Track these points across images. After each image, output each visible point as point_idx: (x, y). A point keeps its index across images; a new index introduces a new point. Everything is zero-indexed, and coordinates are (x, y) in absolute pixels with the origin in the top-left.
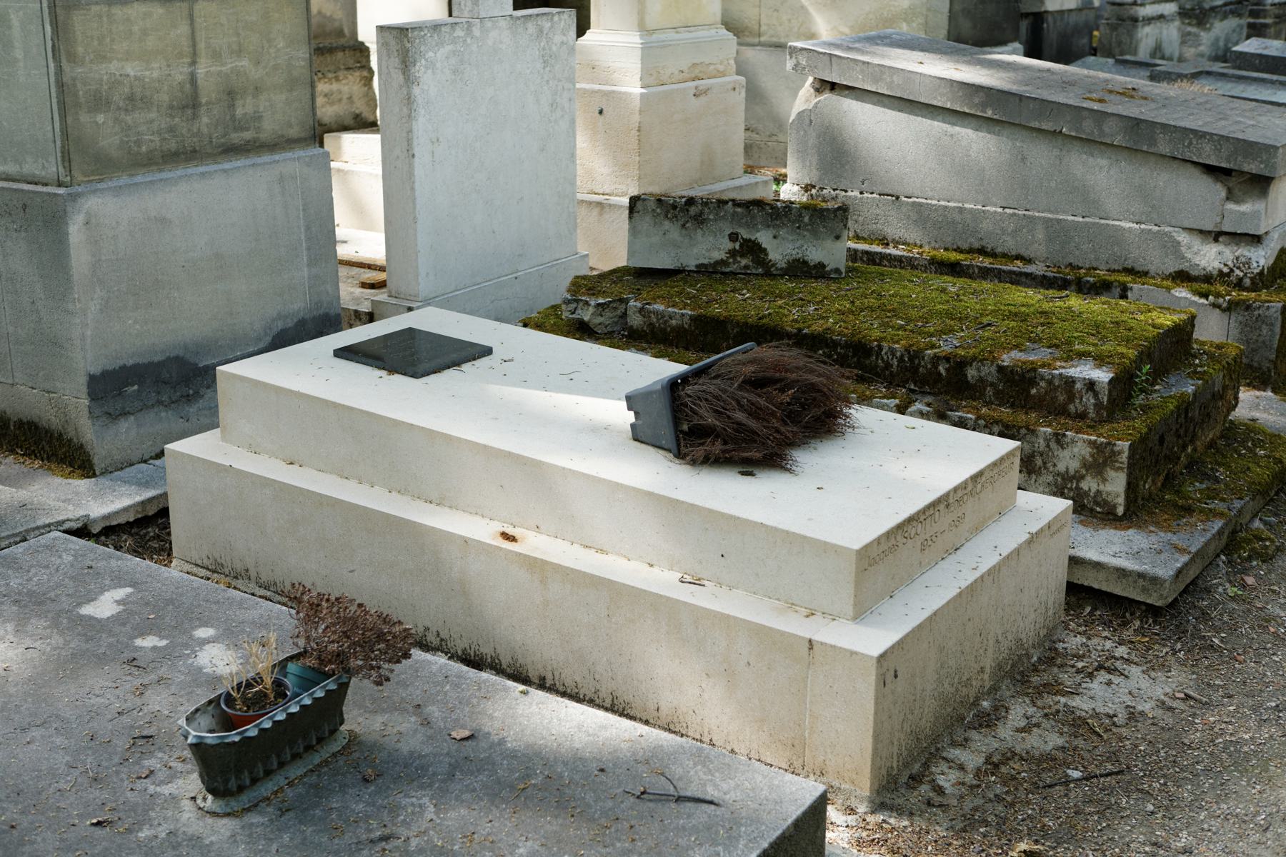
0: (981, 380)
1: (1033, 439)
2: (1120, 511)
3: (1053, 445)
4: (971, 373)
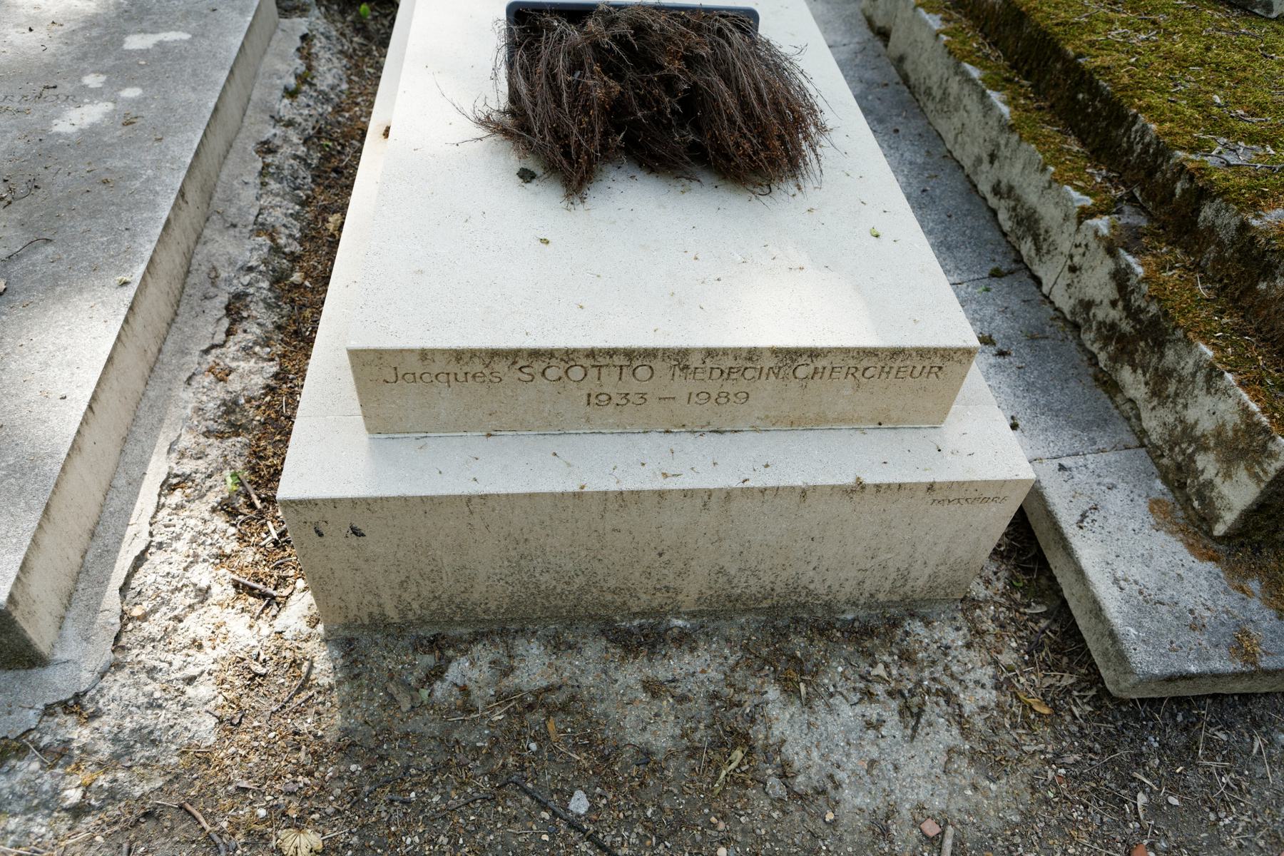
0: (1211, 229)
1: (1184, 353)
2: (1220, 529)
3: (1200, 378)
4: (1207, 212)
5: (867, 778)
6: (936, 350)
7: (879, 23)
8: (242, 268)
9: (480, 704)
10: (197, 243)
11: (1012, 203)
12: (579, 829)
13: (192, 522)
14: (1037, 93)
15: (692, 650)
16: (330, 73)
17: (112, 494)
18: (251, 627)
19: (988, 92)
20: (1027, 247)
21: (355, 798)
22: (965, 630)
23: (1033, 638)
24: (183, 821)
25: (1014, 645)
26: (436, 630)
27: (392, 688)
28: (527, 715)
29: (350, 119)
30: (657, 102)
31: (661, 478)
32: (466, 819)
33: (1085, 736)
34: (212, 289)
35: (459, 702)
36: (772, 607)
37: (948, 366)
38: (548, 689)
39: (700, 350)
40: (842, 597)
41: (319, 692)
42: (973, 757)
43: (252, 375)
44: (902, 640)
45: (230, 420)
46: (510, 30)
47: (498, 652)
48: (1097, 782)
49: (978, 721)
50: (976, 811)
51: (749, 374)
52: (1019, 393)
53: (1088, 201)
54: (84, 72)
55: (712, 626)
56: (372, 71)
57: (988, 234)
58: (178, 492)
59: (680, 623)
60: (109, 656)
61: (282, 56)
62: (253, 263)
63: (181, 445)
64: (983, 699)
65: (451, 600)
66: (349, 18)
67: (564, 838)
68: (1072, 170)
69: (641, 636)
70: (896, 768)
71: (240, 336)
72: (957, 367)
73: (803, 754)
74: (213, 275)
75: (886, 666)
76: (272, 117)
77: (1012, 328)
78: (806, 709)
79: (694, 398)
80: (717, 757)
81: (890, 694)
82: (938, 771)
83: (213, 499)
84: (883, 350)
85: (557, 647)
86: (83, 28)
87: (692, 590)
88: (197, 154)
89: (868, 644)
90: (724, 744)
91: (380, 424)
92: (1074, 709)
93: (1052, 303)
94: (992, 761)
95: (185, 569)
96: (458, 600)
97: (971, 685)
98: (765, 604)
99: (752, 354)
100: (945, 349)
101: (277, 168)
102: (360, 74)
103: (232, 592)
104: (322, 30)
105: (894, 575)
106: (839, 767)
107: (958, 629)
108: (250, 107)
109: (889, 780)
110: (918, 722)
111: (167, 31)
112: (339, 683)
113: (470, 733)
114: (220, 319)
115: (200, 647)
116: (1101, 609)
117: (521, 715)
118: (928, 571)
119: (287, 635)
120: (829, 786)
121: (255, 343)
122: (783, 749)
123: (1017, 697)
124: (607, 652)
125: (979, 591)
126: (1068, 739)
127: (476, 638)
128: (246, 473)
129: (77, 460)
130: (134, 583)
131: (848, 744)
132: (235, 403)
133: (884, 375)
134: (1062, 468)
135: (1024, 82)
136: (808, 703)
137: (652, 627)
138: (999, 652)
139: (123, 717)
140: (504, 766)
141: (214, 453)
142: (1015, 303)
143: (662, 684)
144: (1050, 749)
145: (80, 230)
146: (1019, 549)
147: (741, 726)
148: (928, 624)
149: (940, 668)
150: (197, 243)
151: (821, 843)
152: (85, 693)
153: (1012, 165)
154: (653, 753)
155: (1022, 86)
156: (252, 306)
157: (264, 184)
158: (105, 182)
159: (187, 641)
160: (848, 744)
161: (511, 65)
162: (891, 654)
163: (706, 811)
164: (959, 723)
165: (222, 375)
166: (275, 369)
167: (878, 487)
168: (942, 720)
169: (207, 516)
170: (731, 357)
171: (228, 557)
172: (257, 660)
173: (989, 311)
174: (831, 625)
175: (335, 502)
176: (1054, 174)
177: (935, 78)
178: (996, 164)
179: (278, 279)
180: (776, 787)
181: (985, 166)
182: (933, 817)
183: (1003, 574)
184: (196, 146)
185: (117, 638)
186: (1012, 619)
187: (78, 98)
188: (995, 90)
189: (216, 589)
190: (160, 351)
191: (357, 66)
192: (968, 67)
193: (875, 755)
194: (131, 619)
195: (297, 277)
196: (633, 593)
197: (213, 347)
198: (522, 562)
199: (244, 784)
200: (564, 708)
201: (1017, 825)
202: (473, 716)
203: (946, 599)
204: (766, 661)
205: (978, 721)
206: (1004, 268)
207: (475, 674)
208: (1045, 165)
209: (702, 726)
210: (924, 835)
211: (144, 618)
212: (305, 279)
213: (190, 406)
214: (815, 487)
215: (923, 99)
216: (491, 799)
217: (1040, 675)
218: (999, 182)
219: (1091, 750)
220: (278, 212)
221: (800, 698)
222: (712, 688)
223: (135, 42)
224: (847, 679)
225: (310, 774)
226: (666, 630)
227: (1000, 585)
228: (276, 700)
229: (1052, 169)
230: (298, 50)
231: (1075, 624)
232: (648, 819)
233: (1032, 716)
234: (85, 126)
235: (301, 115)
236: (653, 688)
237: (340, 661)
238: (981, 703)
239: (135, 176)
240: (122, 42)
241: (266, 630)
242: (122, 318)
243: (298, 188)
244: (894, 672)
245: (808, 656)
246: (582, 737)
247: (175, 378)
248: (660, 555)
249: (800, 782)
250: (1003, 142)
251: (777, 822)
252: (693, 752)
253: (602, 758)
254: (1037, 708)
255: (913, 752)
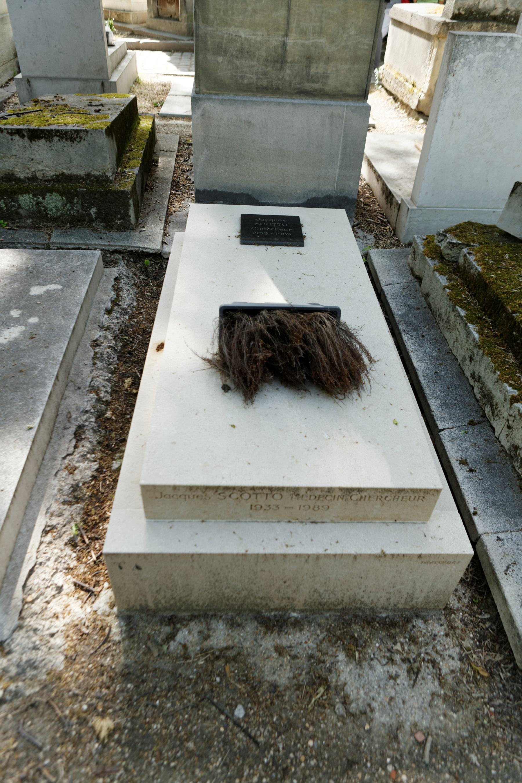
5: (388, 707)
6: (420, 490)
7: (417, 273)
8: (82, 411)
9: (192, 655)
10: (62, 399)
11: (481, 385)
12: (239, 726)
13: (56, 551)
14: (494, 326)
15: (301, 630)
16: (128, 298)
17: (20, 537)
18: (82, 607)
19: (469, 324)
20: (487, 410)
21: (129, 702)
22: (445, 626)
23: (482, 633)
24: (48, 709)
25: (471, 636)
26: (172, 613)
27: (149, 644)
28: (216, 662)
29: (137, 323)
30: (290, 358)
31: (285, 547)
32: (184, 717)
33: (506, 690)
34: (68, 424)
35: (182, 653)
36: (343, 609)
37: (427, 496)
38: (227, 648)
39: (305, 488)
40: (379, 605)
41: (114, 644)
42: (445, 699)
43: (86, 469)
44: (411, 630)
45: (74, 496)
46: (220, 322)
47: (202, 627)
48: (510, 717)
49: (449, 679)
50: (445, 729)
51: (328, 498)
52: (479, 494)
53: (516, 393)
54: (11, 309)
55: (312, 617)
56: (149, 294)
57: (468, 400)
58: (49, 535)
59: (295, 615)
60: (16, 622)
61: (105, 291)
62: (88, 409)
63: (51, 510)
64: (453, 666)
65: (180, 599)
66: (138, 265)
67: (231, 730)
68: (508, 374)
69: (275, 621)
70: (404, 702)
71: (81, 449)
72: (432, 497)
73: (355, 691)
74: (69, 416)
75: (402, 644)
76: (99, 326)
77: (478, 456)
78: (358, 667)
79: (302, 507)
80: (311, 690)
81: (403, 660)
82: (426, 705)
83: (66, 538)
84: (394, 489)
85: (232, 625)
86: (10, 283)
87: (301, 599)
88: (65, 355)
89: (393, 631)
90: (314, 683)
91: (152, 514)
92: (501, 674)
93: (500, 442)
94: (455, 701)
95: (52, 576)
96: (184, 600)
97: (447, 657)
98: (339, 607)
99: (330, 490)
100: (425, 489)
101: (101, 354)
102: (143, 296)
103: (73, 588)
104: (125, 273)
105: (405, 596)
106: (373, 699)
107: (442, 625)
108: (89, 321)
109: (400, 709)
110: (417, 677)
111: (51, 284)
112: (124, 640)
113: (187, 670)
114: (71, 440)
115: (57, 617)
116: (513, 621)
117: (213, 662)
118: (423, 595)
119: (99, 612)
120: (368, 710)
121: (88, 453)
122: (345, 688)
123: (471, 666)
124: (257, 629)
125: (454, 603)
126: (497, 691)
127: (193, 618)
128: (82, 524)
129: (8, 523)
130: (29, 583)
131: (379, 687)
132: (77, 485)
133: (395, 500)
134: (499, 539)
135: (488, 319)
136: (359, 663)
137: (281, 616)
138: (463, 640)
139: (22, 654)
140: (203, 689)
141: (67, 514)
142: (480, 441)
143: (284, 648)
144: (487, 696)
145: (10, 398)
146: (477, 581)
147: (324, 674)
148: (426, 621)
149: (430, 647)
150: (62, 399)
151: (362, 741)
152: (5, 641)
153: (480, 365)
154: (278, 687)
155: (487, 322)
156: (87, 432)
157: (94, 364)
158: (21, 371)
159: (52, 614)
160: (379, 687)
161: (220, 337)
162: (405, 638)
163: (304, 720)
164: (439, 679)
165: (72, 470)
166: (97, 466)
167: (393, 555)
168: (430, 677)
169: (62, 547)
170: (320, 491)
171: (72, 569)
172: (84, 625)
173: (466, 445)
174: (374, 620)
175: (129, 555)
176: (499, 376)
177: (443, 310)
178: (473, 363)
179: (100, 415)
180: (340, 709)
181: (468, 362)
182: (422, 731)
183: (468, 595)
184: (64, 350)
185: (21, 613)
186: (471, 621)
187: (8, 323)
188: (472, 323)
189: (65, 587)
190: (43, 459)
191: (141, 291)
192: (459, 309)
193: (393, 694)
194: (27, 603)
195: (109, 414)
196: (271, 600)
197: (68, 455)
198: (217, 584)
199: (77, 692)
200: (234, 659)
201: (466, 738)
202: (189, 661)
203: (435, 608)
204: (339, 638)
205: (449, 679)
206: (476, 420)
207: (190, 638)
208: (495, 370)
209: (304, 673)
210: (416, 740)
211: (32, 602)
212: (112, 415)
213: (56, 488)
214: (361, 555)
215: (438, 319)
216: (196, 707)
217: (484, 653)
218: (474, 373)
219: (508, 698)
220: (100, 379)
221: (355, 660)
222: (310, 652)
223: (36, 291)
224: (381, 651)
225: (108, 688)
226: (288, 619)
227: (466, 601)
228: (93, 648)
229: (498, 373)
230: (113, 286)
231: (503, 627)
232: (273, 723)
233: (478, 677)
234: (11, 340)
235: (113, 323)
236: (280, 650)
237: (124, 628)
238: (451, 668)
239: (35, 368)
240: (29, 291)
241: (89, 610)
242: (29, 447)
243: (111, 364)
244: (406, 648)
245: (360, 636)
246: (243, 676)
247: (50, 473)
248: (285, 582)
249: (353, 707)
250: (475, 352)
251: (339, 728)
252: (299, 687)
253: (252, 688)
254: (481, 673)
255: (413, 694)
